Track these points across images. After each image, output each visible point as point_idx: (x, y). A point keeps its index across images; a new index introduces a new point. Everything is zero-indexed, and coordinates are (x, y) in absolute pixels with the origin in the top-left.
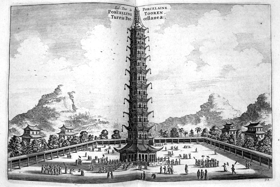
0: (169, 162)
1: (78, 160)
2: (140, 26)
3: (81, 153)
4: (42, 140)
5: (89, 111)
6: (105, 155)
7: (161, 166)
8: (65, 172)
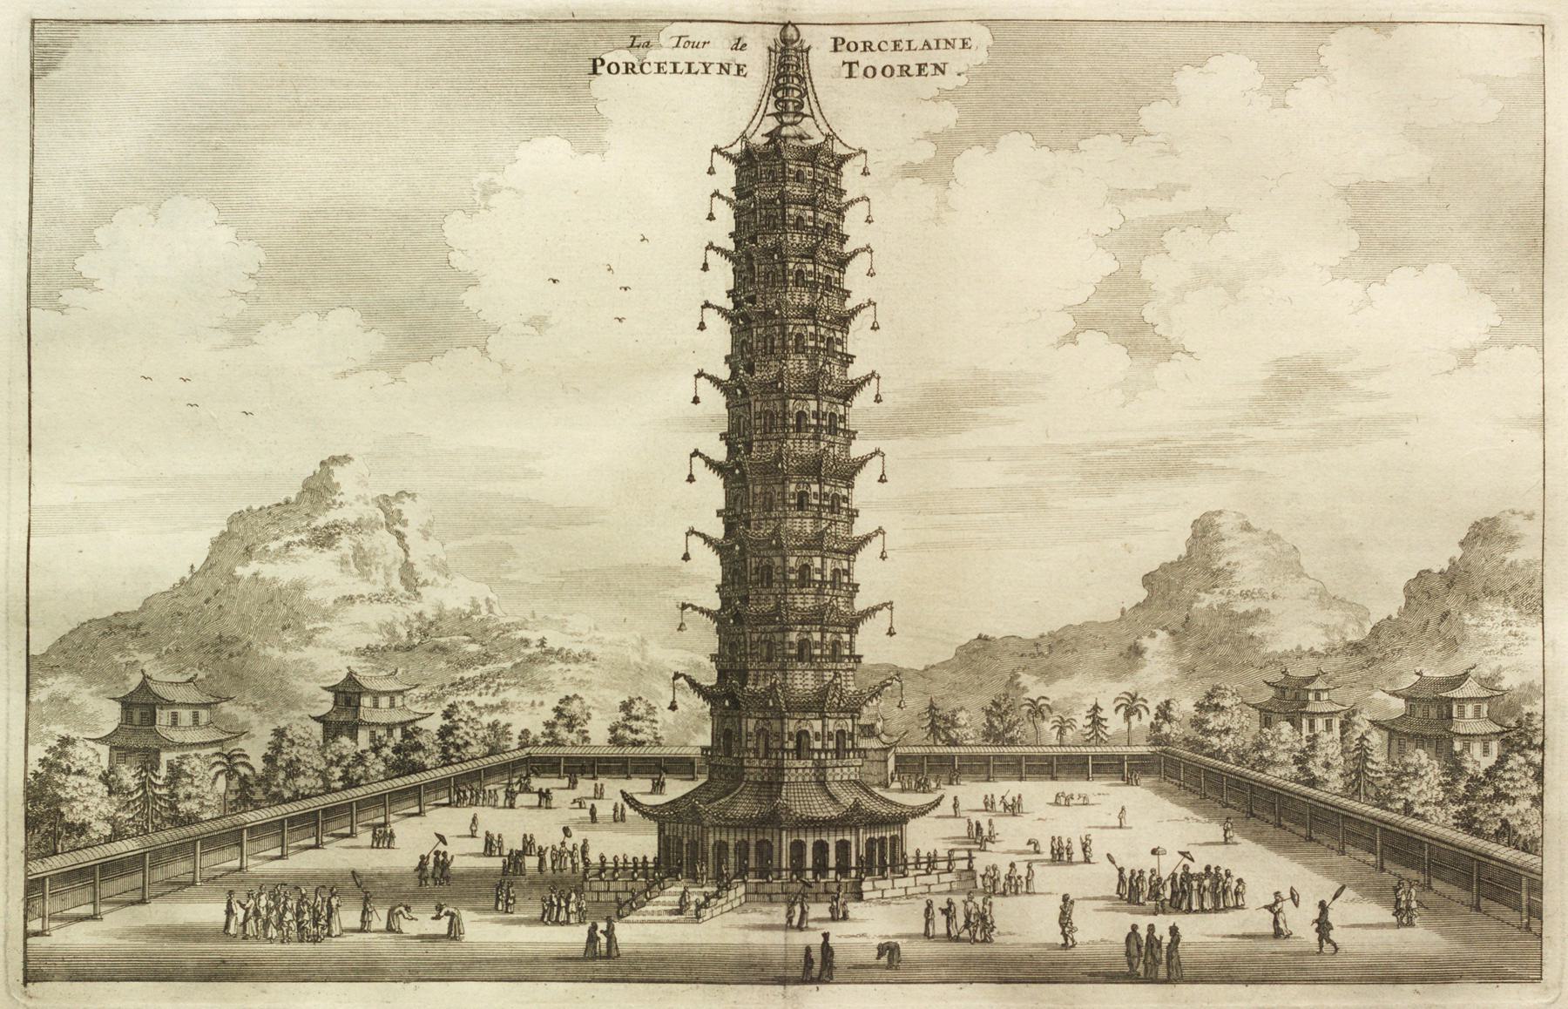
0: (974, 878)
1: (432, 856)
2: (813, 131)
4: (229, 758)
5: (491, 596)
6: (573, 831)
7: (928, 897)
8: (358, 925)
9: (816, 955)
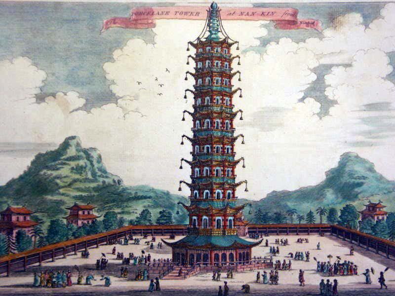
3: (107, 249)
9: (223, 289)
